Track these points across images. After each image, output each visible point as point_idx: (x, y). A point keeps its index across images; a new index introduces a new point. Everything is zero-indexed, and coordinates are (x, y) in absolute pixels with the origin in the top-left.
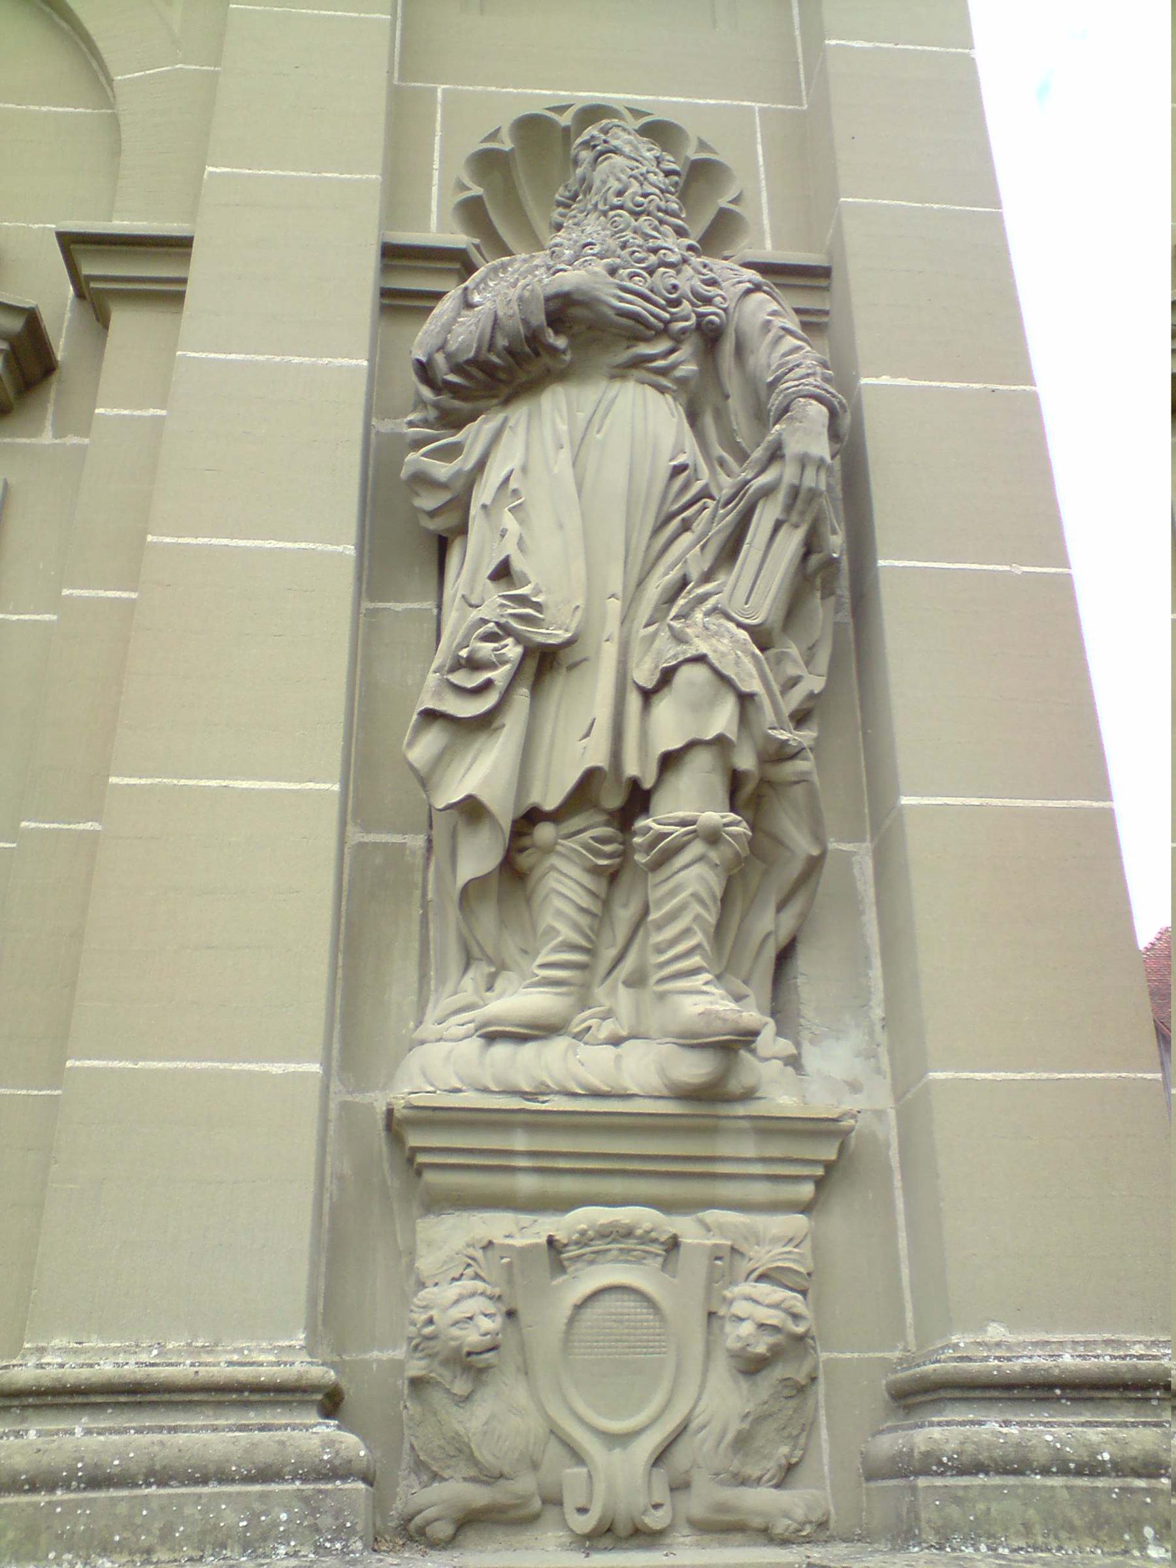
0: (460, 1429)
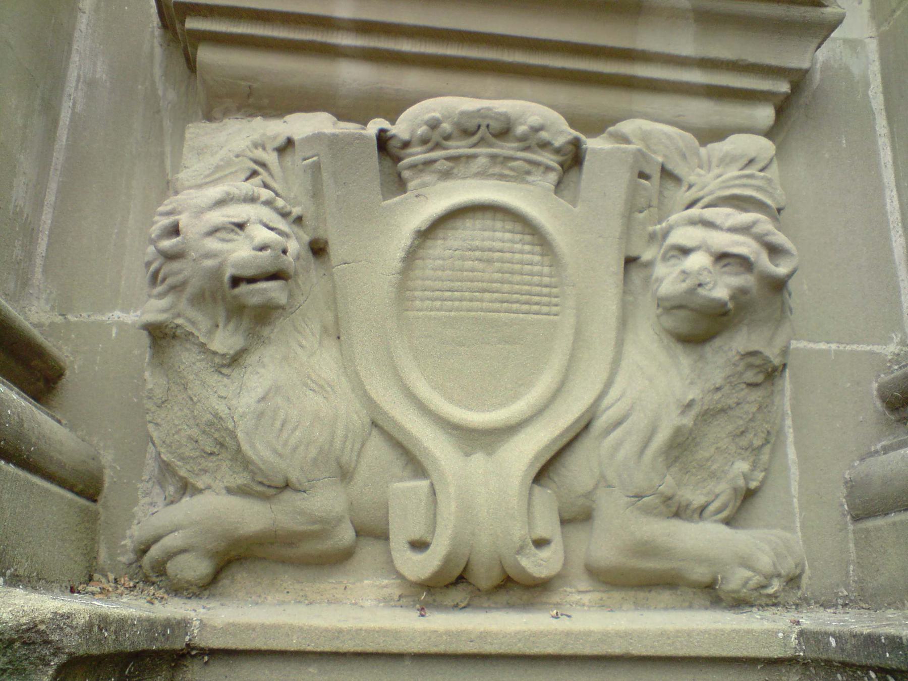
0: (222, 408)
